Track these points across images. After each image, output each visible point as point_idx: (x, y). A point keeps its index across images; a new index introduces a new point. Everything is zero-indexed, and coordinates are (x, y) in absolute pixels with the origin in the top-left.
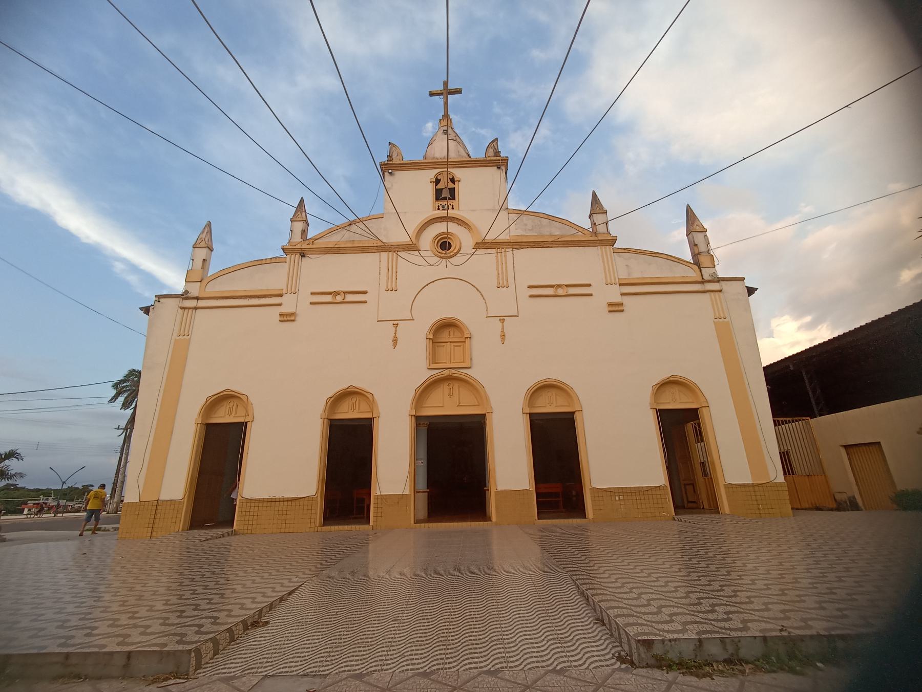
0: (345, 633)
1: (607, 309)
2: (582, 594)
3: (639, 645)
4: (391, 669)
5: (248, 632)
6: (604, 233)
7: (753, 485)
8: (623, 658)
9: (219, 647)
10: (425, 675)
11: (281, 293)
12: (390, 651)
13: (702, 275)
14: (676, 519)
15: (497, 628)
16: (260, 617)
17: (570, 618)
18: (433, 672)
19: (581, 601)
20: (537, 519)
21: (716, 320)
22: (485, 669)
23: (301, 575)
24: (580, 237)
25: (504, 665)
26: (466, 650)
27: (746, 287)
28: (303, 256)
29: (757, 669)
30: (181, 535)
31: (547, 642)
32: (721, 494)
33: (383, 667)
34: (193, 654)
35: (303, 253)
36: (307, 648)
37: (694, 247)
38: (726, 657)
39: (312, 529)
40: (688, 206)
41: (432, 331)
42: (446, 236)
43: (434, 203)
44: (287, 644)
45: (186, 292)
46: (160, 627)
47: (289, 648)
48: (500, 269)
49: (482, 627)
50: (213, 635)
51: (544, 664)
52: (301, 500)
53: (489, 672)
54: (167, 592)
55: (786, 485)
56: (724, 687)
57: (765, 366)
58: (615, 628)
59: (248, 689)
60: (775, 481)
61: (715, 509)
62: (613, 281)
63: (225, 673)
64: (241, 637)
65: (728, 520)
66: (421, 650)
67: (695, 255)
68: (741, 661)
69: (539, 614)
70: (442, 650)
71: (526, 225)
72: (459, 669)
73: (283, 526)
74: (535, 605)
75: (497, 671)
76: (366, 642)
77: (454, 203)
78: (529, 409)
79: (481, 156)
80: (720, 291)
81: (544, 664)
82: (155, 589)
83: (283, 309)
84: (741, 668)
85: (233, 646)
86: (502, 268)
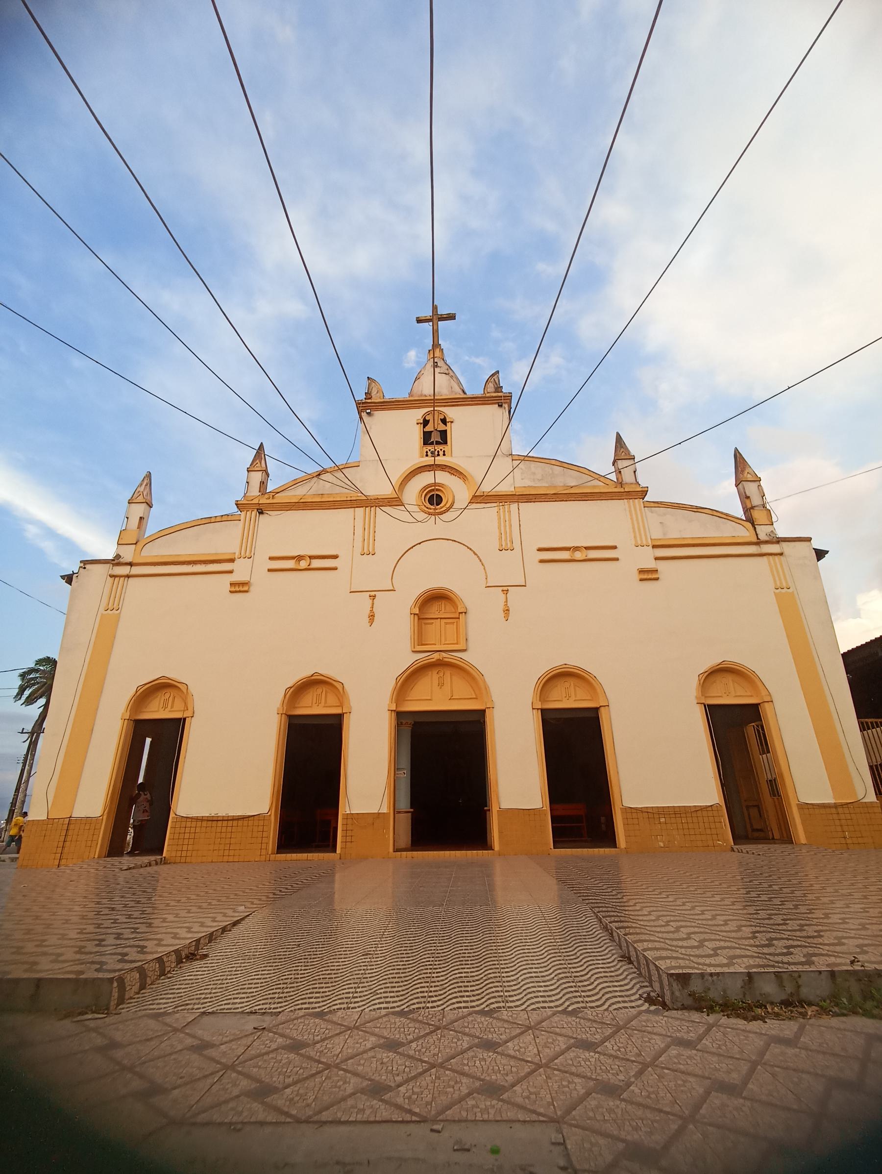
0: (303, 968)
1: (636, 576)
2: (605, 928)
3: (671, 980)
4: (359, 1007)
5: (182, 965)
6: (632, 484)
7: (836, 806)
8: (653, 999)
9: (146, 981)
10: (402, 1014)
11: (233, 557)
12: (359, 988)
13: (757, 535)
14: (735, 849)
15: (498, 991)
16: (197, 948)
17: (588, 954)
18: (411, 1012)
19: (604, 936)
20: (552, 847)
21: (777, 591)
22: (477, 1009)
23: (248, 905)
24: (599, 486)
25: (502, 1004)
26: (455, 988)
27: (814, 549)
28: (261, 513)
29: (824, 1011)
30: (98, 863)
31: (558, 981)
32: (794, 818)
33: (350, 1005)
34: (115, 984)
35: (261, 509)
36: (255, 984)
37: (745, 499)
38: (784, 997)
39: (263, 858)
40: (736, 450)
41: (418, 605)
42: (433, 488)
43: (421, 449)
44: (230, 979)
45: (118, 556)
46: (74, 955)
47: (233, 984)
48: (502, 528)
49: (476, 963)
50: (140, 964)
51: (552, 1004)
52: (250, 819)
53: (482, 1013)
54: (81, 921)
55: (879, 805)
56: (778, 1030)
57: (846, 651)
58: (644, 964)
59: (183, 1025)
60: (864, 801)
61: (787, 838)
62: (644, 543)
63: (154, 1009)
64: (173, 971)
65: (804, 851)
66: (398, 987)
67: (748, 510)
68: (802, 1003)
69: (560, 974)
70: (424, 987)
71: (534, 474)
72: (445, 1008)
73: (226, 853)
74: (554, 961)
75: (493, 1011)
76: (329, 978)
77: (446, 448)
78: (540, 703)
79: (479, 391)
80: (781, 554)
81: (552, 1004)
82: (66, 918)
83: (234, 578)
84: (803, 1010)
85: (164, 981)
86: (505, 526)
